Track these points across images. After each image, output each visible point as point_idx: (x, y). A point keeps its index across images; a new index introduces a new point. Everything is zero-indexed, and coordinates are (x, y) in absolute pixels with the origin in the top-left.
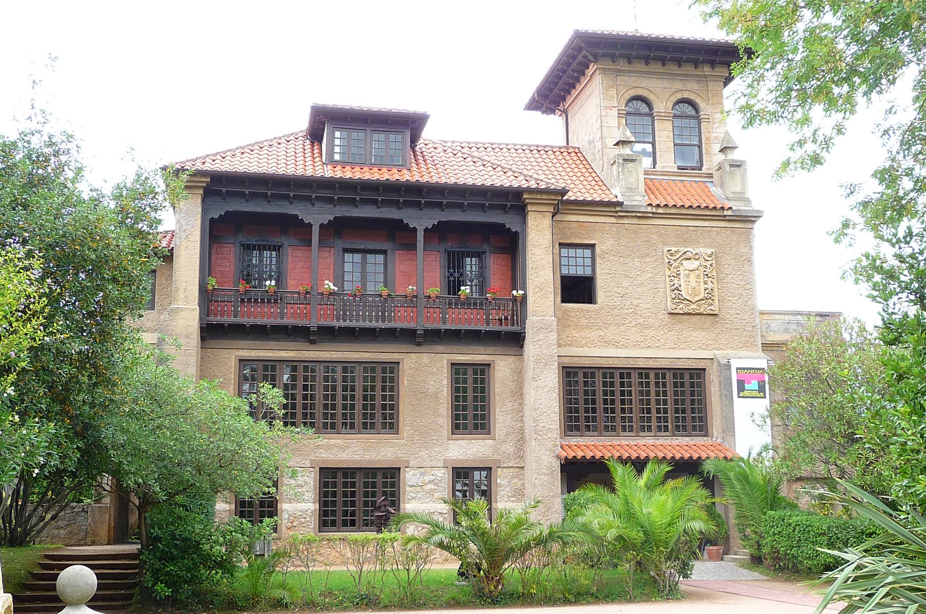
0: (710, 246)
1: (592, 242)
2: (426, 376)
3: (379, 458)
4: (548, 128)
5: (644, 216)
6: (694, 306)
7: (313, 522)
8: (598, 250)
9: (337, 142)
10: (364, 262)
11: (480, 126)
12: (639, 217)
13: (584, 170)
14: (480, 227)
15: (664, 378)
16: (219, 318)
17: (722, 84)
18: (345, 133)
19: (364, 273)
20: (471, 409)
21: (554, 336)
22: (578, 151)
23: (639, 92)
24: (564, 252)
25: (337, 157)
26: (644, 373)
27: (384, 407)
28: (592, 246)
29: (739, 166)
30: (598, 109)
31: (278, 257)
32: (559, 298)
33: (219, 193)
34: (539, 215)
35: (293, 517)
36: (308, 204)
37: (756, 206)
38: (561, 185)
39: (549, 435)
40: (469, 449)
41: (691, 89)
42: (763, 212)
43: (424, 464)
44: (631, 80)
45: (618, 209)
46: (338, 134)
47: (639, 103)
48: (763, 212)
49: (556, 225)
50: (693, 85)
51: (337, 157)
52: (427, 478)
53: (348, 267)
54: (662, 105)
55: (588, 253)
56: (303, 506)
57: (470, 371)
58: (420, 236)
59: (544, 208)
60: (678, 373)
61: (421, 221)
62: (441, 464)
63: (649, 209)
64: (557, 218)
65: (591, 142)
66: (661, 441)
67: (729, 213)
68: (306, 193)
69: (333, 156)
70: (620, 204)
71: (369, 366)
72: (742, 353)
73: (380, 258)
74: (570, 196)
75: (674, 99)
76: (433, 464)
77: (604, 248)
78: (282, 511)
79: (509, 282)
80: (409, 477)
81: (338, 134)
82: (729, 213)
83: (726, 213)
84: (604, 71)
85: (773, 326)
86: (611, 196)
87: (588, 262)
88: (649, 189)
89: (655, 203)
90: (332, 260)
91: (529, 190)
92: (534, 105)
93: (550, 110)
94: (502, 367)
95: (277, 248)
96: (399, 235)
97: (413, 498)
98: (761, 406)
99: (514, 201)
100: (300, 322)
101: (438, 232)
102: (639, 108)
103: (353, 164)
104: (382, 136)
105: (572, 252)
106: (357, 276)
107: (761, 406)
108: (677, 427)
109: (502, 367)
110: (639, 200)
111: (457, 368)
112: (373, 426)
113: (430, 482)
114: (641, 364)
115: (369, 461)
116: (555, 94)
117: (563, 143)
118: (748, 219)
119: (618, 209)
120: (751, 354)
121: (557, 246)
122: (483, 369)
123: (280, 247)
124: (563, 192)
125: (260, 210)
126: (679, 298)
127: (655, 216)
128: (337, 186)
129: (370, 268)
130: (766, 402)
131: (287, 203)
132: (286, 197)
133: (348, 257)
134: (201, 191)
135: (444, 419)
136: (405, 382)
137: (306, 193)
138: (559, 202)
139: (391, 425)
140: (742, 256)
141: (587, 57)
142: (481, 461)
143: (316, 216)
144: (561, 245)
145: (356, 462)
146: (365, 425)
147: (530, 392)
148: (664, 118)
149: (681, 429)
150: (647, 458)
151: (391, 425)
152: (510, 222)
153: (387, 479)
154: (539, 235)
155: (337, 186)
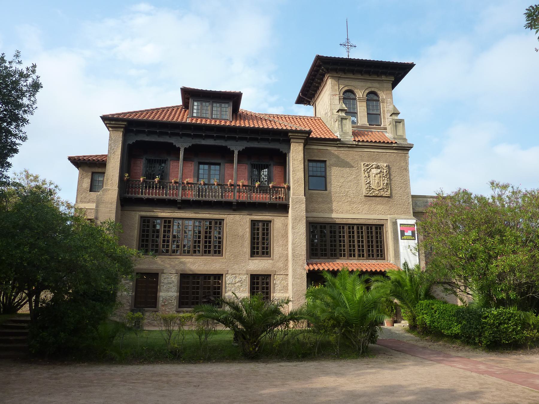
0: (386, 162)
1: (325, 159)
4: (305, 110)
5: (351, 147)
6: (377, 192)
7: (175, 303)
8: (328, 163)
10: (209, 170)
11: (268, 96)
12: (349, 147)
13: (322, 126)
14: (266, 146)
15: (362, 229)
16: (130, 195)
17: (390, 85)
18: (199, 103)
19: (209, 175)
20: (260, 244)
21: (304, 206)
22: (320, 119)
24: (311, 164)
25: (195, 115)
26: (351, 226)
28: (325, 161)
29: (400, 122)
30: (329, 95)
33: (132, 131)
35: (165, 300)
36: (179, 138)
37: (409, 141)
38: (307, 129)
39: (301, 258)
40: (259, 265)
41: (374, 86)
42: (413, 145)
43: (236, 272)
44: (347, 82)
45: (338, 142)
46: (196, 104)
48: (413, 145)
49: (305, 150)
50: (376, 85)
51: (195, 115)
52: (237, 280)
53: (201, 171)
54: (360, 94)
55: (323, 165)
59: (300, 141)
60: (369, 226)
61: (236, 148)
62: (244, 272)
63: (354, 143)
64: (307, 147)
65: (326, 114)
66: (361, 262)
67: (395, 145)
68: (177, 131)
70: (339, 140)
72: (403, 216)
73: (217, 167)
74: (313, 135)
75: (367, 92)
76: (241, 272)
77: (331, 162)
78: (160, 296)
79: (283, 179)
80: (228, 279)
81: (196, 104)
82: (395, 145)
83: (393, 145)
84: (333, 77)
85: (418, 203)
86: (334, 137)
87: (323, 169)
88: (354, 134)
89: (357, 140)
90: (193, 168)
91: (292, 131)
93: (308, 103)
96: (225, 155)
98: (413, 243)
102: (348, 96)
104: (218, 105)
105: (314, 164)
106: (206, 176)
107: (413, 243)
108: (369, 255)
109: (277, 221)
110: (349, 139)
111: (254, 223)
113: (239, 282)
114: (350, 222)
115: (207, 271)
118: (406, 149)
119: (338, 142)
120: (408, 217)
121: (307, 161)
122: (267, 223)
123: (165, 161)
124: (309, 132)
125: (153, 140)
126: (370, 188)
127: (357, 146)
128: (192, 127)
129: (212, 172)
130: (416, 241)
131: (168, 137)
132: (166, 134)
133: (201, 166)
135: (247, 249)
137: (177, 131)
138: (308, 139)
139: (218, 251)
140: (402, 167)
141: (324, 68)
142: (265, 271)
143: (182, 144)
144: (309, 161)
147: (291, 234)
148: (361, 100)
149: (370, 256)
150: (338, 270)
151: (218, 251)
152: (281, 147)
154: (296, 155)
155: (192, 127)
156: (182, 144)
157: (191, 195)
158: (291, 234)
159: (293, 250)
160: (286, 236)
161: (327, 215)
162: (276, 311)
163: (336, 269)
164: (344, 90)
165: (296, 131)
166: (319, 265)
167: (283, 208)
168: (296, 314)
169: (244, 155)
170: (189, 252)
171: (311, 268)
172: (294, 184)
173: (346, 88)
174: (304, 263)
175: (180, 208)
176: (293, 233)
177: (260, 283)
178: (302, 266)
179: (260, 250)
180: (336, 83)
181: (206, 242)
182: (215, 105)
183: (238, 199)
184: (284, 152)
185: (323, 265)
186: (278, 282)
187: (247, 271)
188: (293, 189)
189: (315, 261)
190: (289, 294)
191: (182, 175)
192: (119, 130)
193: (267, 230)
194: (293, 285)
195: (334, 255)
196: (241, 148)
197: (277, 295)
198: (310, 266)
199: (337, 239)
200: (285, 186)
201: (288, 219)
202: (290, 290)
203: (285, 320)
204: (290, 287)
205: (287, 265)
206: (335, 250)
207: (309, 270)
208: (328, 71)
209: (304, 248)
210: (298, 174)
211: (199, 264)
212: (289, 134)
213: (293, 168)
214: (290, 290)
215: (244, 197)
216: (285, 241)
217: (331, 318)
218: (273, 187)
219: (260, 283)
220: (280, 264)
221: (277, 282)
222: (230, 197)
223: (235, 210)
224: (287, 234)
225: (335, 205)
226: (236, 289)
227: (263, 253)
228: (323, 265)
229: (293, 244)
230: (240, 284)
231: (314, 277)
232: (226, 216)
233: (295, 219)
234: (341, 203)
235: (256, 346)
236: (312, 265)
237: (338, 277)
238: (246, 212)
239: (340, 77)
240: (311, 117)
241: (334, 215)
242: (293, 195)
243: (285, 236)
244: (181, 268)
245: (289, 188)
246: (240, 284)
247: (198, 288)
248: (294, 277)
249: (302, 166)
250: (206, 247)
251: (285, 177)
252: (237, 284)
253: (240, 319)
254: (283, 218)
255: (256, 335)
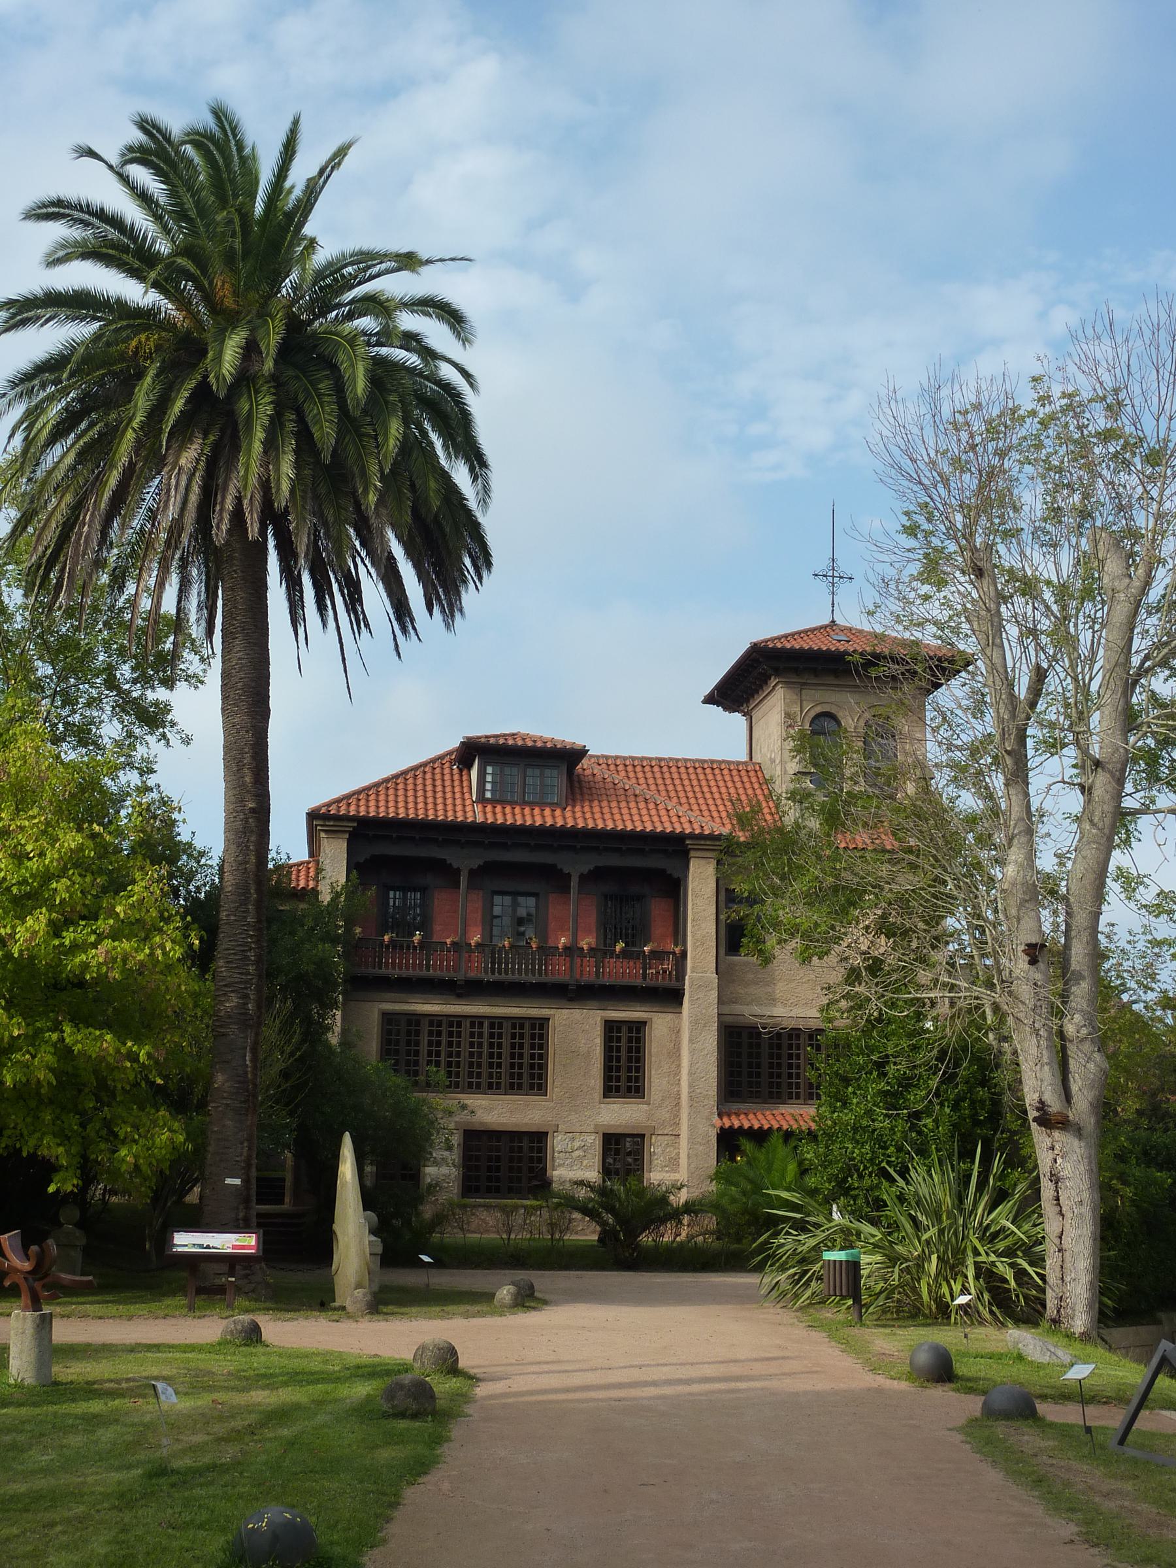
2: (577, 1032)
3: (526, 1121)
4: (722, 736)
9: (489, 778)
14: (637, 873)
20: (624, 1070)
23: (826, 708)
25: (488, 795)
27: (532, 1066)
31: (422, 898)
32: (722, 951)
34: (703, 862)
39: (706, 1102)
40: (621, 1114)
44: (819, 694)
47: (827, 719)
51: (488, 795)
52: (577, 1144)
56: (444, 1170)
57: (624, 1029)
58: (574, 883)
59: (708, 854)
61: (576, 866)
62: (591, 1129)
69: (484, 794)
71: (517, 1022)
76: (583, 1128)
80: (558, 1143)
81: (489, 770)
84: (787, 684)
91: (692, 836)
92: (710, 700)
94: (659, 1024)
95: (423, 890)
96: (556, 880)
97: (560, 1165)
99: (676, 847)
100: (446, 975)
101: (593, 877)
103: (503, 802)
104: (537, 772)
109: (659, 1024)
111: (610, 1027)
112: (520, 1087)
115: (516, 1125)
116: (737, 690)
117: (744, 758)
133: (497, 899)
134: (347, 836)
135: (596, 1081)
136: (555, 1040)
145: (502, 1124)
146: (512, 1086)
147: (684, 1051)
149: (258, 1194)
150: (770, 1129)
152: (669, 865)
153: (532, 1146)
154: (701, 882)
156: (465, 860)
157: (476, 968)
158: (684, 1051)
159: (690, 1086)
160: (675, 1054)
161: (758, 1010)
162: (663, 1200)
163: (766, 1127)
164: (813, 714)
165: (701, 837)
166: (742, 1116)
167: (671, 996)
168: (694, 1204)
169: (593, 877)
170: (478, 1086)
171: (727, 1123)
172: (695, 948)
173: (819, 709)
174: (712, 1113)
175: (459, 996)
176: (692, 1052)
177: (623, 1151)
178: (708, 1119)
179: (622, 1084)
180: (795, 697)
181: (512, 1066)
182: (530, 771)
183: (578, 977)
184: (676, 875)
185: (751, 1116)
186: (659, 1150)
187: (596, 1125)
188: (693, 958)
189: (735, 1107)
190: (682, 1176)
191: (463, 924)
192: (340, 835)
193: (638, 1040)
194: (689, 1157)
195: (777, 1094)
196: (585, 869)
197: (657, 1176)
198: (725, 1120)
199: (785, 1061)
200: (677, 950)
201: (681, 1019)
202: (682, 1163)
203: (675, 1215)
204: (683, 1161)
205: (677, 1116)
206: (779, 1085)
207: (722, 1128)
208: (777, 672)
209: (714, 1083)
210: (703, 926)
211: (498, 1111)
212: (688, 842)
213: (693, 963)
214: (682, 1163)
215: (588, 972)
216: (674, 1066)
217: (745, 1211)
218: (651, 952)
219: (623, 1151)
220: (664, 1114)
221: (656, 1149)
222: (559, 970)
223: (571, 1000)
224: (679, 1050)
225: (780, 989)
226: (575, 1165)
227: (629, 1089)
228: (751, 1116)
229: (690, 1074)
230: (582, 1154)
231: (728, 1142)
232: (552, 1012)
233: (695, 1022)
234: (793, 985)
235: (634, 1250)
236: (729, 1116)
237: (763, 1150)
238: (595, 1004)
239: (805, 684)
240: (738, 763)
241: (779, 1011)
242: (693, 972)
243: (675, 1054)
244: (462, 1117)
245: (684, 954)
246: (582, 1154)
247: (498, 1159)
248: (691, 1141)
249: (713, 909)
250: (512, 1076)
251: (678, 930)
252: (576, 1153)
253: (611, 1210)
254: (671, 1016)
255: (633, 1234)
